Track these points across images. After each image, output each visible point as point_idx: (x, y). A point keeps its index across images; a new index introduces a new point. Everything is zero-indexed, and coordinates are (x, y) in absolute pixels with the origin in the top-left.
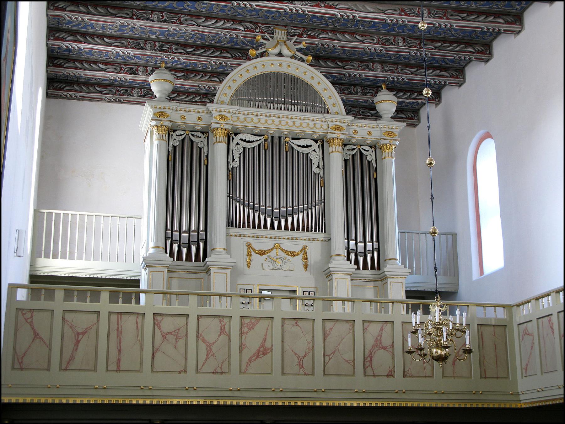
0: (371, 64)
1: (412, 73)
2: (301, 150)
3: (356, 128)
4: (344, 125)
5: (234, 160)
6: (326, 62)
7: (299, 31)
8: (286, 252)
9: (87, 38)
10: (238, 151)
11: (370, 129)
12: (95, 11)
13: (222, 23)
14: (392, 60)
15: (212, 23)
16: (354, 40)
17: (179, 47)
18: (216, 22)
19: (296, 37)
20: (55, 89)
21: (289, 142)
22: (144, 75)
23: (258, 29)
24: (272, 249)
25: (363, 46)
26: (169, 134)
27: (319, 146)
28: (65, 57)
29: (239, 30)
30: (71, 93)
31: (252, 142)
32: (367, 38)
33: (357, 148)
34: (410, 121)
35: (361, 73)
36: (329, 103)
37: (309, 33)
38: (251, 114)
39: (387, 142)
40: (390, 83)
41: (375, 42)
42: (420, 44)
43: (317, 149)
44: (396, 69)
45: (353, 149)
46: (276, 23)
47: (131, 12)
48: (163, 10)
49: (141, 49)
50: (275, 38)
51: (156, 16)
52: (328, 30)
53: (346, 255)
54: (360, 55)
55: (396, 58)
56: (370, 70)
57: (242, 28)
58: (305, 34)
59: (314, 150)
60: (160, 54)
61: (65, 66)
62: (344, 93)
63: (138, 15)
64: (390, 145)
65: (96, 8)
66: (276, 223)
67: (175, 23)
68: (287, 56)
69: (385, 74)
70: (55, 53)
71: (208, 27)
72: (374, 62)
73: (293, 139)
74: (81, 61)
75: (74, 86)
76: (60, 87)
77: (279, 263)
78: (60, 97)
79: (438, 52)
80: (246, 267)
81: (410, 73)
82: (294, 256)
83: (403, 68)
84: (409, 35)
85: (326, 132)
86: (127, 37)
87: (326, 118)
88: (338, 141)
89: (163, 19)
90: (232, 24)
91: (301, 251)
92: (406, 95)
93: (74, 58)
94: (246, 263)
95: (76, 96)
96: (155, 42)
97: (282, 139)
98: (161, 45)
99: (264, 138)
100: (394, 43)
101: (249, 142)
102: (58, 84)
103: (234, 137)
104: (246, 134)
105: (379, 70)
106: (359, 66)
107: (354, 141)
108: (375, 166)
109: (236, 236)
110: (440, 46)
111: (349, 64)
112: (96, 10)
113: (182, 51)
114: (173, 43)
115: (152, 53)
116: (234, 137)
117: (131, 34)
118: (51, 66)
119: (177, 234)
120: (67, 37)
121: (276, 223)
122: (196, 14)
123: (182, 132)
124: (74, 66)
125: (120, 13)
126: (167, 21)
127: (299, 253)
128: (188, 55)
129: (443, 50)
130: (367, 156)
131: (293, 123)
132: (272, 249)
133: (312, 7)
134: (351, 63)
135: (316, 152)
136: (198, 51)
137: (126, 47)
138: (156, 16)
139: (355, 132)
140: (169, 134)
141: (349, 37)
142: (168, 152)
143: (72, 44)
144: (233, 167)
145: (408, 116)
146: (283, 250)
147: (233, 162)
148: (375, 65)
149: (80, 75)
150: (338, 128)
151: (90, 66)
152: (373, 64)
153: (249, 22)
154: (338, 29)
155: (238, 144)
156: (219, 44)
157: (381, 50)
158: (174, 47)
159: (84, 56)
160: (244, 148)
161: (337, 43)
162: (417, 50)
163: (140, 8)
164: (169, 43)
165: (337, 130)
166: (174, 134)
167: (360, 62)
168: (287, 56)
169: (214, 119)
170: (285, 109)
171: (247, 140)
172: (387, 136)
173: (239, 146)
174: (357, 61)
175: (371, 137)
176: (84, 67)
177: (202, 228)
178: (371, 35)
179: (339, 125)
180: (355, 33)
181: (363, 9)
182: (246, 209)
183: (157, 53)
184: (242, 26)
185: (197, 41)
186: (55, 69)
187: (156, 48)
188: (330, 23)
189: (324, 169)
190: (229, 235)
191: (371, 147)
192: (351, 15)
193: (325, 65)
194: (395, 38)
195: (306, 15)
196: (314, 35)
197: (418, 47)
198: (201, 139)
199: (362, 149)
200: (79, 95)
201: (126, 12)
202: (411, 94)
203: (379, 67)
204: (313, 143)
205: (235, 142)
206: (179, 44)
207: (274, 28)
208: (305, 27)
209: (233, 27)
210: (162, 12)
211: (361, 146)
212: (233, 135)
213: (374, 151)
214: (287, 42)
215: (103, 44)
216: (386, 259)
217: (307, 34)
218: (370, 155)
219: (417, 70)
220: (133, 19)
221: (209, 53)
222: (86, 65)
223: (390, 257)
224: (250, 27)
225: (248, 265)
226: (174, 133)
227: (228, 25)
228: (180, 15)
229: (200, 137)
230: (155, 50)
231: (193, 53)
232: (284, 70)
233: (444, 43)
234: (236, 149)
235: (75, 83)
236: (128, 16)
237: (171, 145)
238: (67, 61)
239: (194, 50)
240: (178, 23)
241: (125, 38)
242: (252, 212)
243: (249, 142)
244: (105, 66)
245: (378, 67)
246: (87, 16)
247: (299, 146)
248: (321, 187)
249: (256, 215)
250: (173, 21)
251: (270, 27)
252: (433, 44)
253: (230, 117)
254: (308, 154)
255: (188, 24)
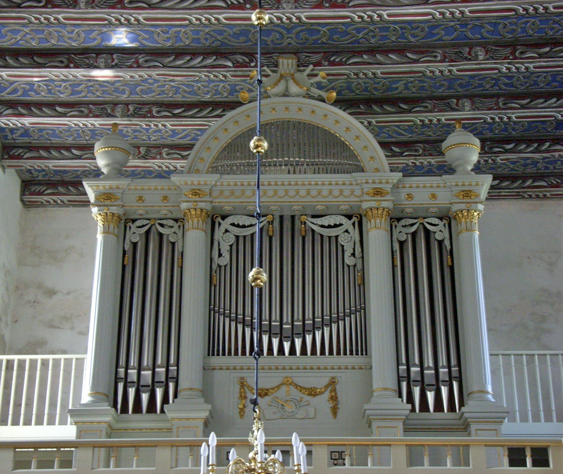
0: (455, 101)
1: (523, 107)
2: (326, 232)
3: (409, 191)
4: (388, 188)
5: (220, 255)
6: (382, 106)
7: (316, 58)
8: (301, 388)
9: (32, 110)
10: (227, 241)
11: (433, 190)
12: (16, 63)
13: (199, 59)
14: (486, 90)
15: (185, 61)
16: (404, 61)
17: (162, 109)
18: (191, 59)
19: (311, 67)
20: (32, 194)
21: (307, 221)
22: (136, 159)
23: (253, 62)
24: (278, 387)
25: (420, 67)
26: (125, 227)
27: (354, 224)
28: (26, 145)
29: (226, 67)
30: (54, 197)
31: (249, 226)
32: (425, 55)
33: (418, 223)
34: (555, 191)
35: (439, 115)
36: (364, 157)
37: (332, 59)
38: (239, 184)
39: (463, 206)
40: (502, 131)
41: (439, 59)
42: (513, 53)
43: (351, 229)
44: (495, 104)
45: (412, 225)
46: (280, 51)
47: (67, 59)
48: (113, 52)
49: (107, 117)
50: (279, 71)
51: (103, 60)
52: (362, 51)
53: (397, 390)
54: (434, 90)
55: (492, 87)
56: (453, 110)
57: (230, 64)
58: (326, 61)
59: (347, 231)
60: (135, 121)
61: (25, 157)
62: (431, 155)
63: (78, 61)
64: (468, 211)
65: (17, 59)
66: (287, 346)
67: (131, 67)
68: (298, 96)
69: (478, 114)
70: (9, 140)
71: (178, 68)
72: (458, 98)
73: (314, 217)
74: (47, 149)
75: (59, 187)
76: (39, 191)
77: (289, 408)
78: (41, 205)
79: (544, 62)
80: (237, 416)
81: (519, 106)
82: (314, 396)
83: (507, 101)
84: (494, 42)
85: (358, 200)
86: (88, 103)
87: (356, 178)
88: (379, 212)
89: (113, 64)
90: (215, 60)
91: (327, 387)
92: (532, 146)
93: (37, 145)
94: (238, 410)
95: (62, 201)
96: (127, 104)
97: (296, 218)
98: (137, 108)
99: (268, 220)
100: (469, 57)
101: (244, 226)
102: (37, 187)
103: (221, 221)
104: (239, 216)
105: (467, 108)
106: (434, 107)
107: (409, 210)
108: (449, 248)
109: (221, 369)
110: (548, 52)
111: (420, 105)
112: (17, 61)
113: (167, 114)
114: (153, 104)
115: (125, 121)
116: (221, 221)
117: (91, 98)
118: (6, 159)
119: (134, 373)
120: (4, 111)
121: (287, 346)
122: (161, 51)
123: (145, 222)
124: (38, 155)
125: (50, 62)
126: (120, 66)
127: (323, 390)
128: (176, 118)
129: (553, 58)
130: (435, 233)
131: (307, 192)
132: (278, 387)
133: (310, 10)
134: (422, 103)
135: (349, 233)
136: (191, 111)
137: (87, 116)
138: (103, 60)
139: (410, 196)
140: (125, 227)
141: (397, 57)
142: (124, 252)
143: (11, 120)
144: (220, 266)
145: (552, 183)
146: (296, 386)
147: (219, 259)
148: (460, 102)
149: (48, 167)
150: (378, 192)
151: (60, 154)
152: (458, 100)
153: (240, 54)
154: (378, 47)
155: (227, 231)
156: (218, 98)
157: (450, 71)
158: (155, 110)
159: (50, 140)
160: (237, 237)
161: (378, 68)
162: (509, 63)
163: (80, 52)
164: (149, 104)
165: (376, 196)
166: (134, 227)
167: (437, 100)
168: (298, 96)
169: (183, 196)
170: (294, 173)
171: (241, 224)
172: (462, 197)
173: (228, 234)
174: (431, 100)
175: (437, 202)
176: (51, 155)
177: (172, 361)
178: (433, 50)
179: (379, 188)
180: (405, 50)
181: (391, 2)
182: (240, 327)
183: (130, 121)
184: (230, 60)
185: (187, 98)
186: (10, 162)
187: (129, 113)
188: (362, 38)
189: (363, 257)
190: (207, 369)
191: (441, 219)
192: (374, 14)
193: (380, 111)
194: (471, 49)
195: (305, 24)
196: (341, 60)
197: (511, 58)
198: (173, 230)
199: (428, 223)
200: (65, 198)
201: (60, 59)
202: (539, 145)
203: (467, 104)
204: (344, 220)
205: (223, 228)
206: (162, 104)
207: (278, 57)
208: (325, 50)
209: (216, 63)
210: (112, 54)
211: (424, 218)
212: (219, 219)
213: (447, 225)
214: (296, 75)
215: (53, 115)
216: (469, 392)
217: (329, 61)
218: (441, 231)
219: (531, 101)
220: (70, 68)
221: (205, 112)
222: (54, 153)
223: (475, 388)
224: (241, 61)
225: (240, 413)
226: (133, 224)
227: (209, 61)
228: (137, 55)
229: (172, 227)
230: (128, 116)
231: (183, 115)
232: (294, 115)
233: (554, 46)
234: (224, 239)
235: (59, 184)
236: (62, 65)
237: (127, 241)
238: (28, 150)
239: (184, 111)
240: (135, 66)
241: (86, 104)
242: (241, 328)
243: (244, 226)
244: (80, 152)
245: (466, 104)
246: (5, 71)
247: (323, 226)
248: (360, 286)
249: (265, 338)
250: (127, 65)
251: (271, 57)
252: (537, 50)
253: (208, 191)
254: (337, 237)
255: (149, 67)
